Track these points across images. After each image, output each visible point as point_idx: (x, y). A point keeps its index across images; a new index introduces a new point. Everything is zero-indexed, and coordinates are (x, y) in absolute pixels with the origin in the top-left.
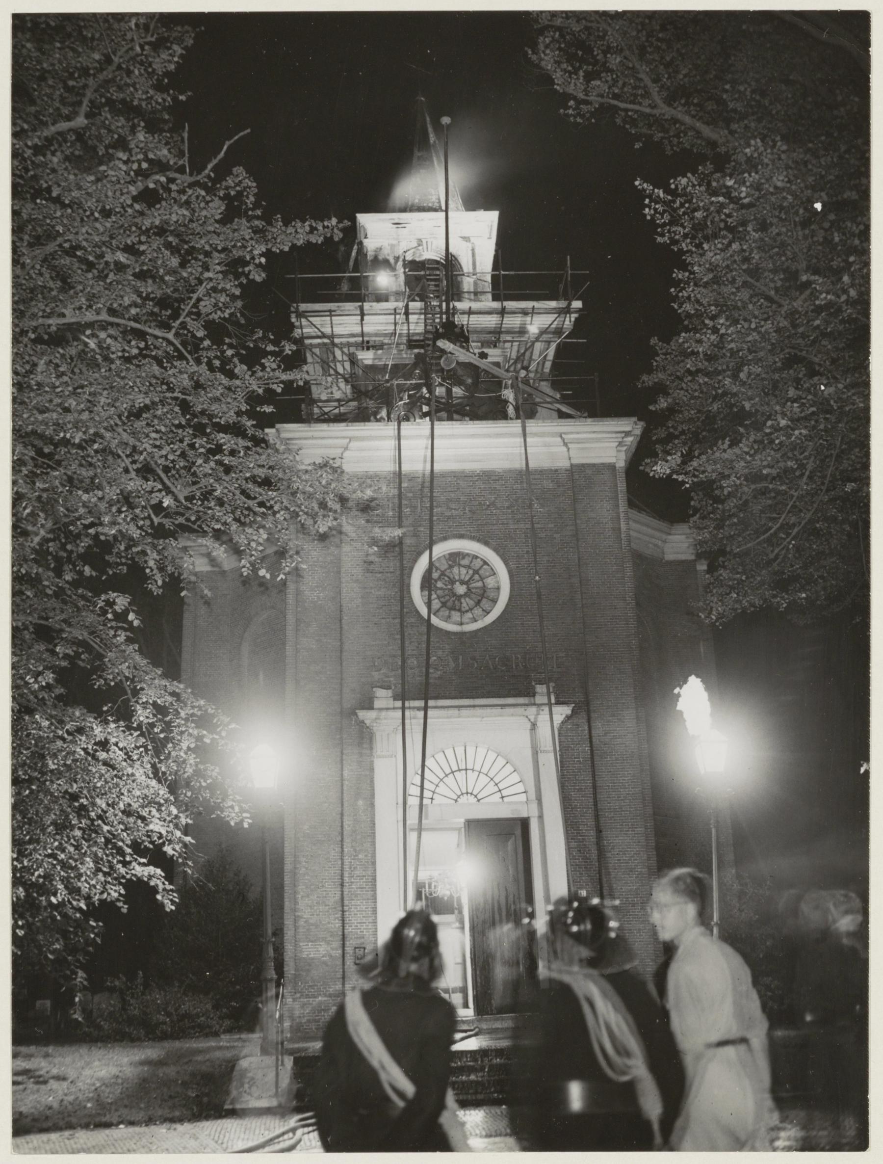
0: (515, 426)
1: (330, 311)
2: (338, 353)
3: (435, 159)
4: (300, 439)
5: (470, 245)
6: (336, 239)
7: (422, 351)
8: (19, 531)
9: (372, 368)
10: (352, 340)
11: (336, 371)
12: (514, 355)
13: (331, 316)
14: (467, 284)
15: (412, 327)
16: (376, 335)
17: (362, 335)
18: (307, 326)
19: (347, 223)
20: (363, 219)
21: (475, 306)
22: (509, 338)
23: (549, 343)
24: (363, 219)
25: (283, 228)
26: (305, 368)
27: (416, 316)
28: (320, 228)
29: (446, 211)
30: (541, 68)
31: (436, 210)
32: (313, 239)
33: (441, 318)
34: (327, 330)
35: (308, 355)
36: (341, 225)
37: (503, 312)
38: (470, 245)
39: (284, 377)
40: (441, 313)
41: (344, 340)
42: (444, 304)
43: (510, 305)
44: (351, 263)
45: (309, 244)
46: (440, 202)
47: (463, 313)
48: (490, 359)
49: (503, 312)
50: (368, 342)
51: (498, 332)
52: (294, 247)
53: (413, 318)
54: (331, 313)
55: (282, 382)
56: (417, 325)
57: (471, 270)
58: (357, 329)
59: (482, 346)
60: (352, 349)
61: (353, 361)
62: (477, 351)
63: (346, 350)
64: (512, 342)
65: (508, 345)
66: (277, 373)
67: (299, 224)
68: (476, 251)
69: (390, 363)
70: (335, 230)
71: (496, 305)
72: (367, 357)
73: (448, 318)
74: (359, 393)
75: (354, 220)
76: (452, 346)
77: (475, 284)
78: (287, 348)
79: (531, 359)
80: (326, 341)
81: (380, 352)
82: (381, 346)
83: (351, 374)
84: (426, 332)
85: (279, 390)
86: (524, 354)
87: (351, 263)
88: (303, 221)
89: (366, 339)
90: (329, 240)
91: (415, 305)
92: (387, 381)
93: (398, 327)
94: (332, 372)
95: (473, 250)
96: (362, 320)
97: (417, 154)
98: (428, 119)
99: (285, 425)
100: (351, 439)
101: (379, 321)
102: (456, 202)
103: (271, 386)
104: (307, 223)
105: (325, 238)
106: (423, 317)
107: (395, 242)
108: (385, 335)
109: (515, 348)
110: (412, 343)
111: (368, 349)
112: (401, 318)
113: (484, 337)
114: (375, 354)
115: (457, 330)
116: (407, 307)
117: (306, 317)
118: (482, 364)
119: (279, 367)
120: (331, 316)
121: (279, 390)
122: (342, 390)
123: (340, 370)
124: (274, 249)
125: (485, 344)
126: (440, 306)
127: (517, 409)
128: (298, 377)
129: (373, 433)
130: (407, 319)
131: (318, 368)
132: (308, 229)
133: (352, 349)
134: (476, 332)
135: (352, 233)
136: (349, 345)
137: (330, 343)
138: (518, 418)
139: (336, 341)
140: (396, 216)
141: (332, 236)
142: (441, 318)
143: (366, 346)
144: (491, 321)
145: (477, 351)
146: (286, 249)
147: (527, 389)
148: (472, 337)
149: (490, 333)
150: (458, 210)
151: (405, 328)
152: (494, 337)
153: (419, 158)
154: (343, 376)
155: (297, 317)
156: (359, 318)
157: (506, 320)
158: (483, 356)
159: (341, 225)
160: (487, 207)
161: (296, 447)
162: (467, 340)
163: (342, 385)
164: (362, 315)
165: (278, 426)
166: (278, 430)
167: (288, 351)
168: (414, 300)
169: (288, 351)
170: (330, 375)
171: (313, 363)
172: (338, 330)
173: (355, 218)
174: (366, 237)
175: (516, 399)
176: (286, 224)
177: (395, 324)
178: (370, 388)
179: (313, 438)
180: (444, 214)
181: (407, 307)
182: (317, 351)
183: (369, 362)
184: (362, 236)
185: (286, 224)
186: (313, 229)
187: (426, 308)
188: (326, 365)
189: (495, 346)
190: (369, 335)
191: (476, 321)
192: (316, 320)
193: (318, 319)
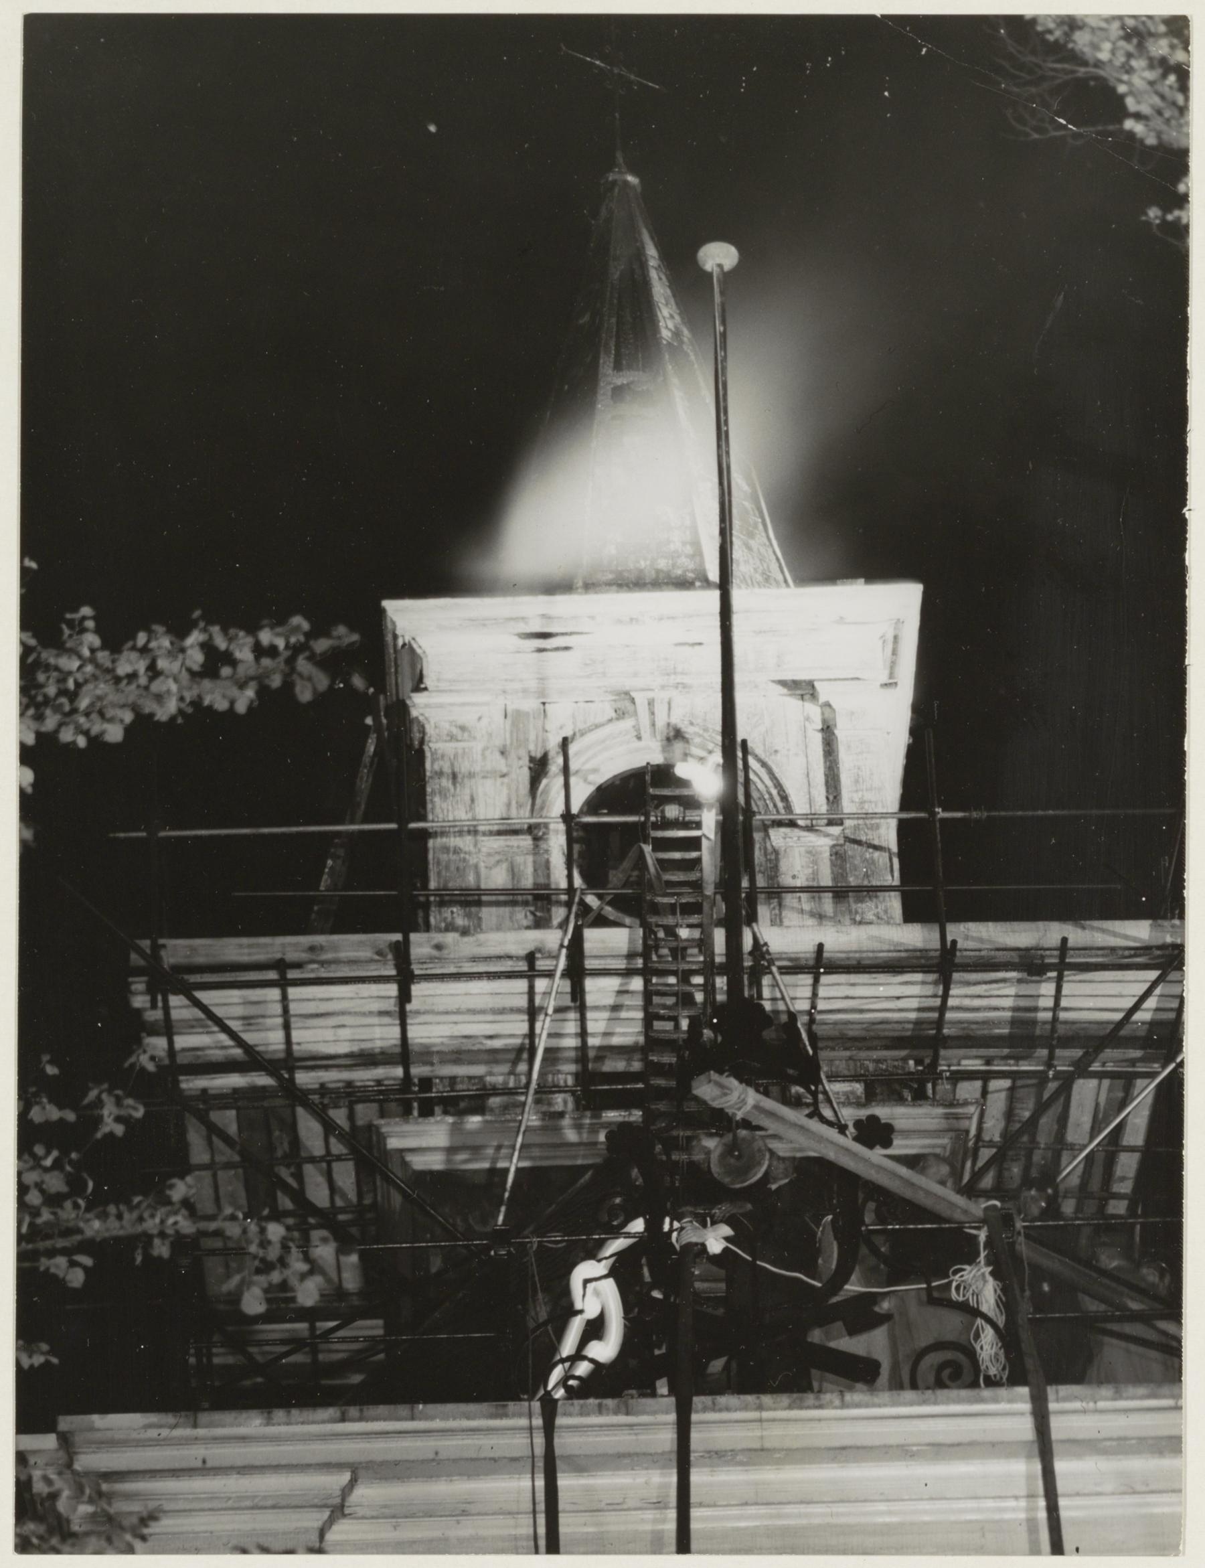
0: (1009, 1414)
1: (281, 965)
2: (310, 1130)
3: (675, 381)
4: (153, 1473)
5: (814, 711)
6: (304, 695)
7: (636, 1115)
8: (57, 1551)
9: (444, 1184)
10: (364, 1076)
11: (298, 1195)
12: (994, 1128)
13: (283, 984)
14: (800, 856)
15: (597, 1023)
16: (458, 1055)
17: (404, 1054)
18: (190, 1026)
19: (345, 636)
20: (410, 618)
21: (841, 939)
22: (973, 1064)
23: (1126, 1081)
24: (410, 618)
25: (103, 657)
26: (179, 1190)
27: (614, 983)
28: (244, 654)
29: (724, 586)
30: (1076, 58)
31: (683, 584)
32: (216, 697)
33: (709, 988)
34: (271, 1039)
35: (195, 1137)
36: (321, 645)
37: (944, 965)
38: (814, 711)
39: (94, 1227)
40: (709, 969)
41: (332, 1077)
42: (719, 937)
43: (974, 935)
44: (364, 781)
45: (199, 713)
46: (698, 553)
47: (795, 967)
48: (901, 1146)
49: (944, 965)
50: (426, 1083)
51: (927, 1038)
52: (142, 724)
53: (599, 990)
54: (283, 974)
55: (87, 1246)
56: (614, 1015)
57: (822, 806)
58: (385, 1035)
59: (870, 1097)
60: (365, 1112)
61: (369, 1154)
62: (848, 1115)
63: (339, 1115)
64: (985, 1077)
65: (968, 1090)
66: (68, 1213)
67: (164, 642)
68: (840, 733)
69: (513, 1164)
70: (302, 664)
71: (916, 936)
72: (425, 1142)
73: (734, 988)
74: (384, 1288)
75: (374, 627)
76: (752, 1097)
77: (838, 856)
78: (109, 1111)
79: (1060, 1144)
80: (263, 1080)
81: (475, 1121)
82: (475, 1099)
83: (359, 1209)
84: (652, 1042)
85: (77, 1278)
86: (1032, 1124)
87: (364, 781)
88: (180, 631)
89: (417, 1071)
90: (274, 701)
91: (610, 942)
92: (500, 1237)
93: (544, 1026)
94: (286, 1203)
95: (828, 731)
96: (404, 997)
97: (610, 377)
98: (651, 251)
99: (97, 1420)
100: (357, 1471)
101: (465, 1008)
102: (759, 547)
103: (44, 1263)
104: (195, 638)
105: (263, 691)
106: (637, 984)
107: (530, 704)
108: (493, 1056)
109: (997, 1103)
110: (594, 1084)
111: (427, 1111)
112: (552, 990)
113: (870, 1059)
114: (456, 1129)
115: (769, 1034)
116: (576, 948)
117: (187, 991)
118: (873, 1162)
119: (75, 1186)
120: (283, 984)
121: (77, 1278)
122: (323, 1269)
123: (318, 1194)
124: (66, 736)
125: (882, 1086)
126: (704, 944)
127: (1008, 1338)
128: (151, 1225)
129: (450, 1446)
130: (578, 993)
131: (232, 1183)
132: (196, 658)
133: (365, 1112)
134: (847, 1039)
135: (378, 674)
136: (351, 1094)
137: (282, 1084)
138: (1016, 1378)
139: (303, 1078)
140: (533, 609)
141: (288, 685)
142: (709, 988)
143: (417, 1097)
144: (900, 998)
145: (848, 1115)
146: (114, 734)
147: (1051, 1262)
148: (832, 1059)
149: (897, 1042)
150: (767, 580)
151: (571, 1026)
152: (914, 1059)
153: (618, 392)
154: (327, 1219)
155: (151, 991)
156: (392, 990)
157: (959, 995)
158: (874, 1133)
159: (321, 645)
160: (872, 562)
161: (136, 1507)
162: (809, 1074)
163: (325, 1252)
164: (405, 979)
165: (65, 1423)
166: (65, 1440)
167: (110, 1126)
168: (601, 921)
169: (110, 1126)
170: (277, 1216)
171: (210, 1166)
172: (307, 1038)
173: (382, 612)
174: (419, 685)
175: (1007, 1302)
176: (114, 642)
177: (533, 1012)
178: (436, 1264)
179: (205, 1469)
180: (713, 598)
181: (576, 948)
182: (228, 1120)
183: (436, 1162)
184: (408, 684)
185: (114, 642)
186: (215, 661)
187: (649, 948)
188: (266, 1172)
189: (920, 1096)
190: (427, 1054)
191: (843, 998)
192: (227, 1002)
193: (235, 995)
